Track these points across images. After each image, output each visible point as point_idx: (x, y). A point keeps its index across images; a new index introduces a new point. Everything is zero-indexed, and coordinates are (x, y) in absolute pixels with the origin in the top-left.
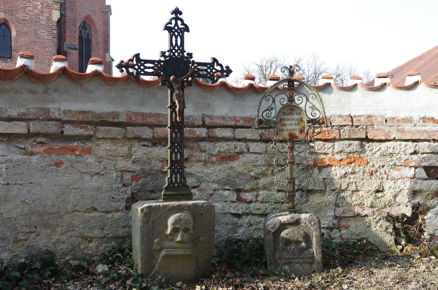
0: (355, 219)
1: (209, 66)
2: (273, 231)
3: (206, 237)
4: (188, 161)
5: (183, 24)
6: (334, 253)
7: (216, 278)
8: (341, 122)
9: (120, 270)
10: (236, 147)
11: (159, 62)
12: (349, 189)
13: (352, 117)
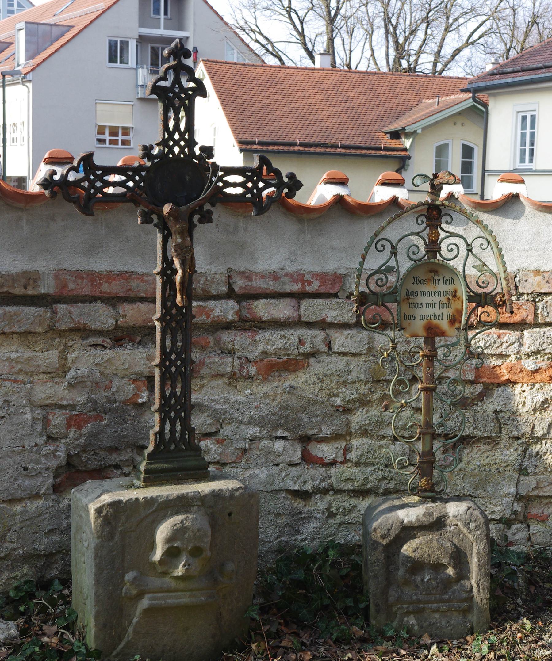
1: (249, 174)
6: (513, 582)
7: (259, 653)
8: (539, 284)
9: (44, 634)
10: (301, 342)
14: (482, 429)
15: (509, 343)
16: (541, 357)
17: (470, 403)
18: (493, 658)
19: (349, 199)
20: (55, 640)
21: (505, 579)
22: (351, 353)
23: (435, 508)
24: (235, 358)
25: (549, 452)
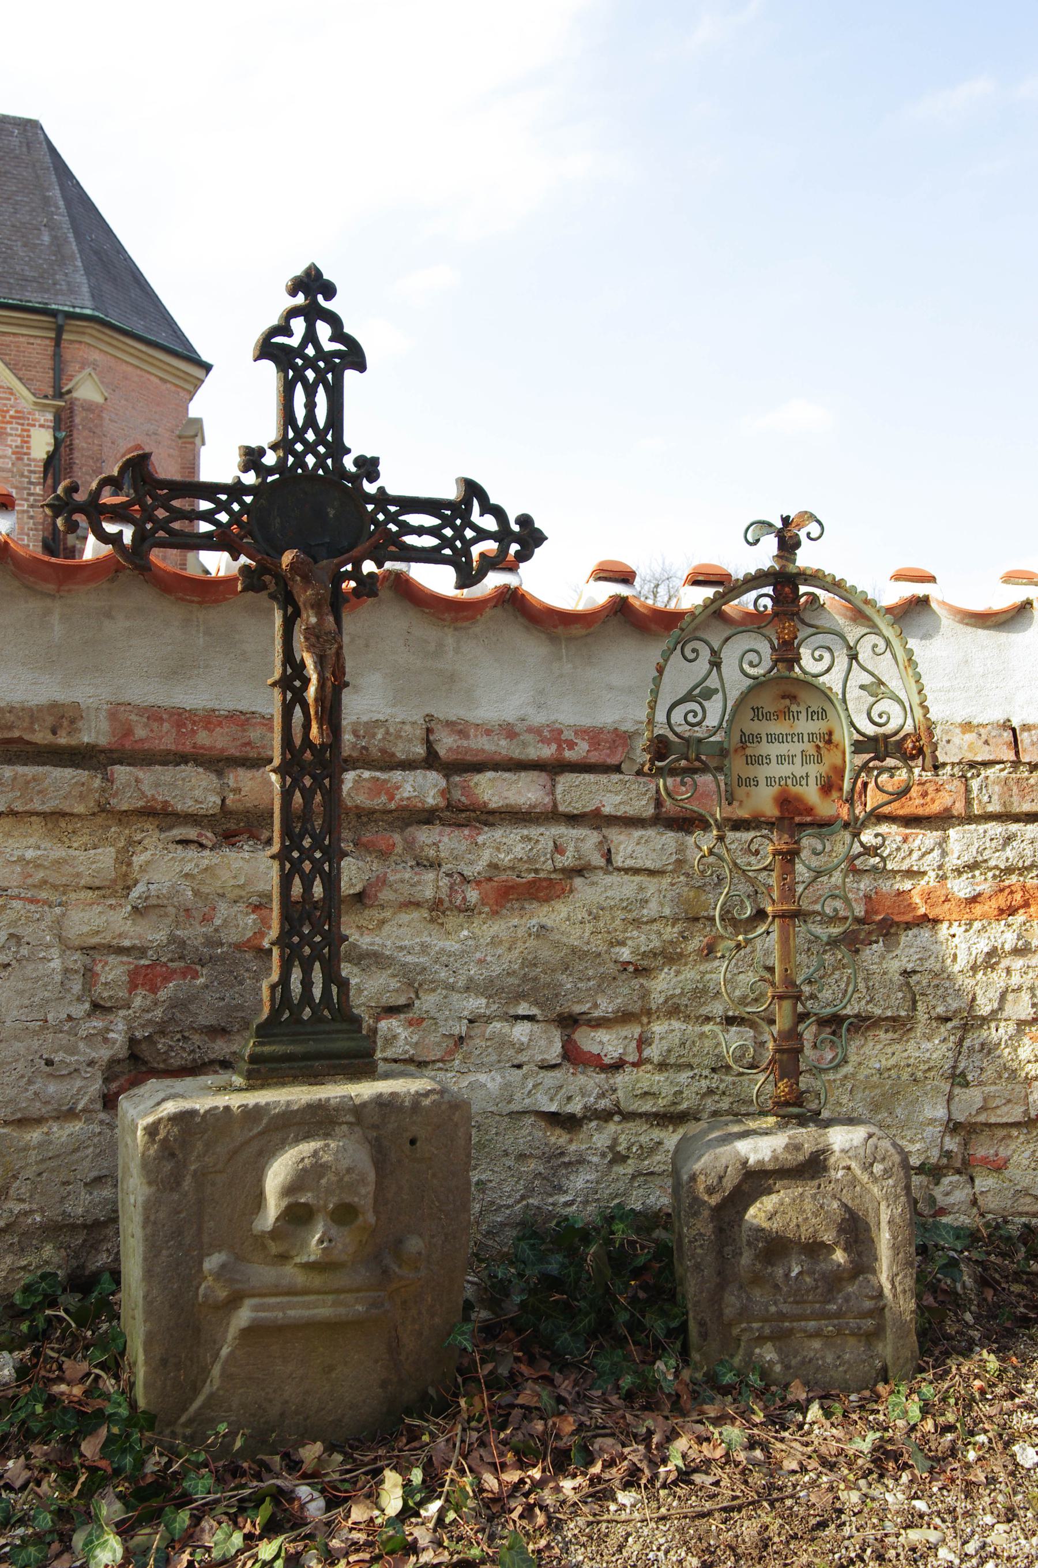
0: (1029, 1133)
2: (714, 1201)
3: (433, 1237)
4: (365, 906)
5: (339, 334)
6: (954, 1281)
8: (971, 747)
10: (558, 849)
11: (236, 490)
12: (1005, 1015)
13: (1014, 730)
14: (882, 1003)
15: (923, 850)
16: (981, 874)
17: (863, 940)
18: (933, 1431)
19: (636, 604)
20: (77, 1391)
21: (939, 1276)
22: (645, 870)
23: (807, 1136)
24: (441, 874)
25: (1003, 1043)
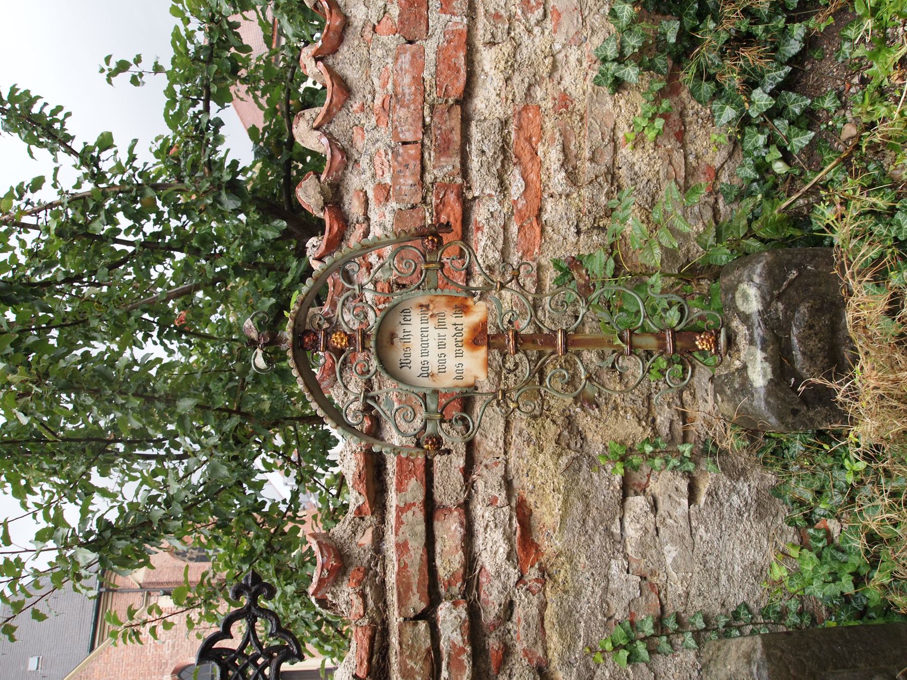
10: (493, 502)
